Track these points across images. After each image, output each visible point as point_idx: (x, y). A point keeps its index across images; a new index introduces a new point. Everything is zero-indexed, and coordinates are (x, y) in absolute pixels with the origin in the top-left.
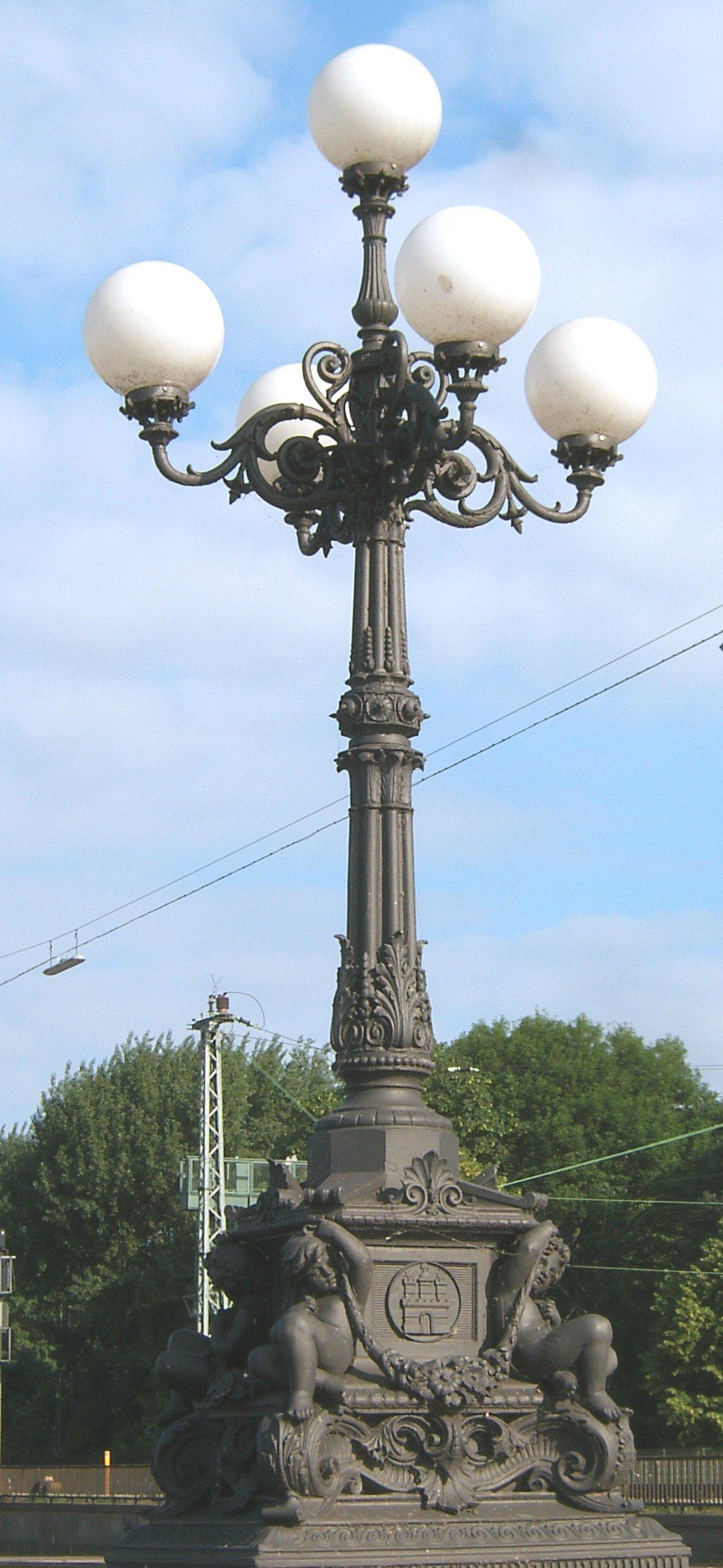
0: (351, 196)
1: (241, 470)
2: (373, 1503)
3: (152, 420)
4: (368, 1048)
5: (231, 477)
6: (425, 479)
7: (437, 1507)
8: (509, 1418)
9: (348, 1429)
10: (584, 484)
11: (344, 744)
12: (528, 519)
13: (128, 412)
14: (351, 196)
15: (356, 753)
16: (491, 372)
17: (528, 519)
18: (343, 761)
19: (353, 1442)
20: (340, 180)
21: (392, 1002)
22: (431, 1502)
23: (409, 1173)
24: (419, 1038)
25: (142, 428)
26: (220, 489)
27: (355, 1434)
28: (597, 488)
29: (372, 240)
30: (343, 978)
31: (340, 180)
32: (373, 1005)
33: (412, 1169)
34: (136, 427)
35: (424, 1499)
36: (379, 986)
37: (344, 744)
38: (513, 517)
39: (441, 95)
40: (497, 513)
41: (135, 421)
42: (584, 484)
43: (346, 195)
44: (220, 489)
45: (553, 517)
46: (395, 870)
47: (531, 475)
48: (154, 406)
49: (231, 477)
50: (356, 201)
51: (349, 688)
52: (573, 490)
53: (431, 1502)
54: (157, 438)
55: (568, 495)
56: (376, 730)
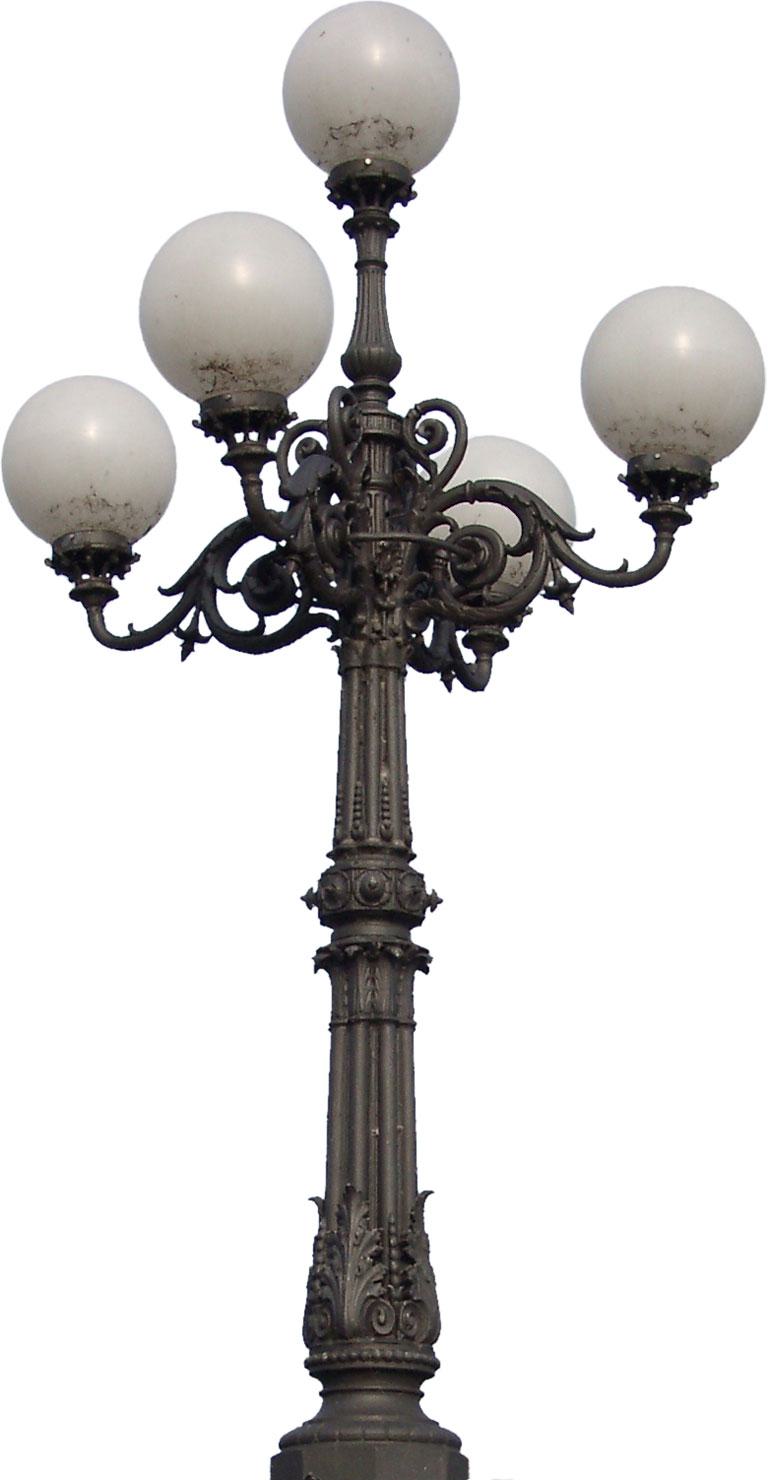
0: (639, 499)
1: (196, 616)
3: (85, 577)
5: (185, 625)
10: (665, 523)
11: (324, 936)
12: (588, 593)
13: (58, 564)
14: (639, 499)
15: (342, 947)
16: (328, 192)
17: (588, 593)
18: (325, 960)
25: (72, 586)
26: (172, 643)
28: (681, 529)
29: (370, 268)
30: (321, 1245)
34: (65, 585)
37: (324, 936)
38: (564, 595)
40: (541, 585)
41: (64, 579)
42: (665, 523)
43: (335, 206)
44: (172, 643)
45: (621, 579)
47: (621, 563)
49: (185, 625)
50: (348, 212)
51: (331, 863)
52: (649, 532)
54: (94, 599)
55: (639, 546)
56: (371, 918)
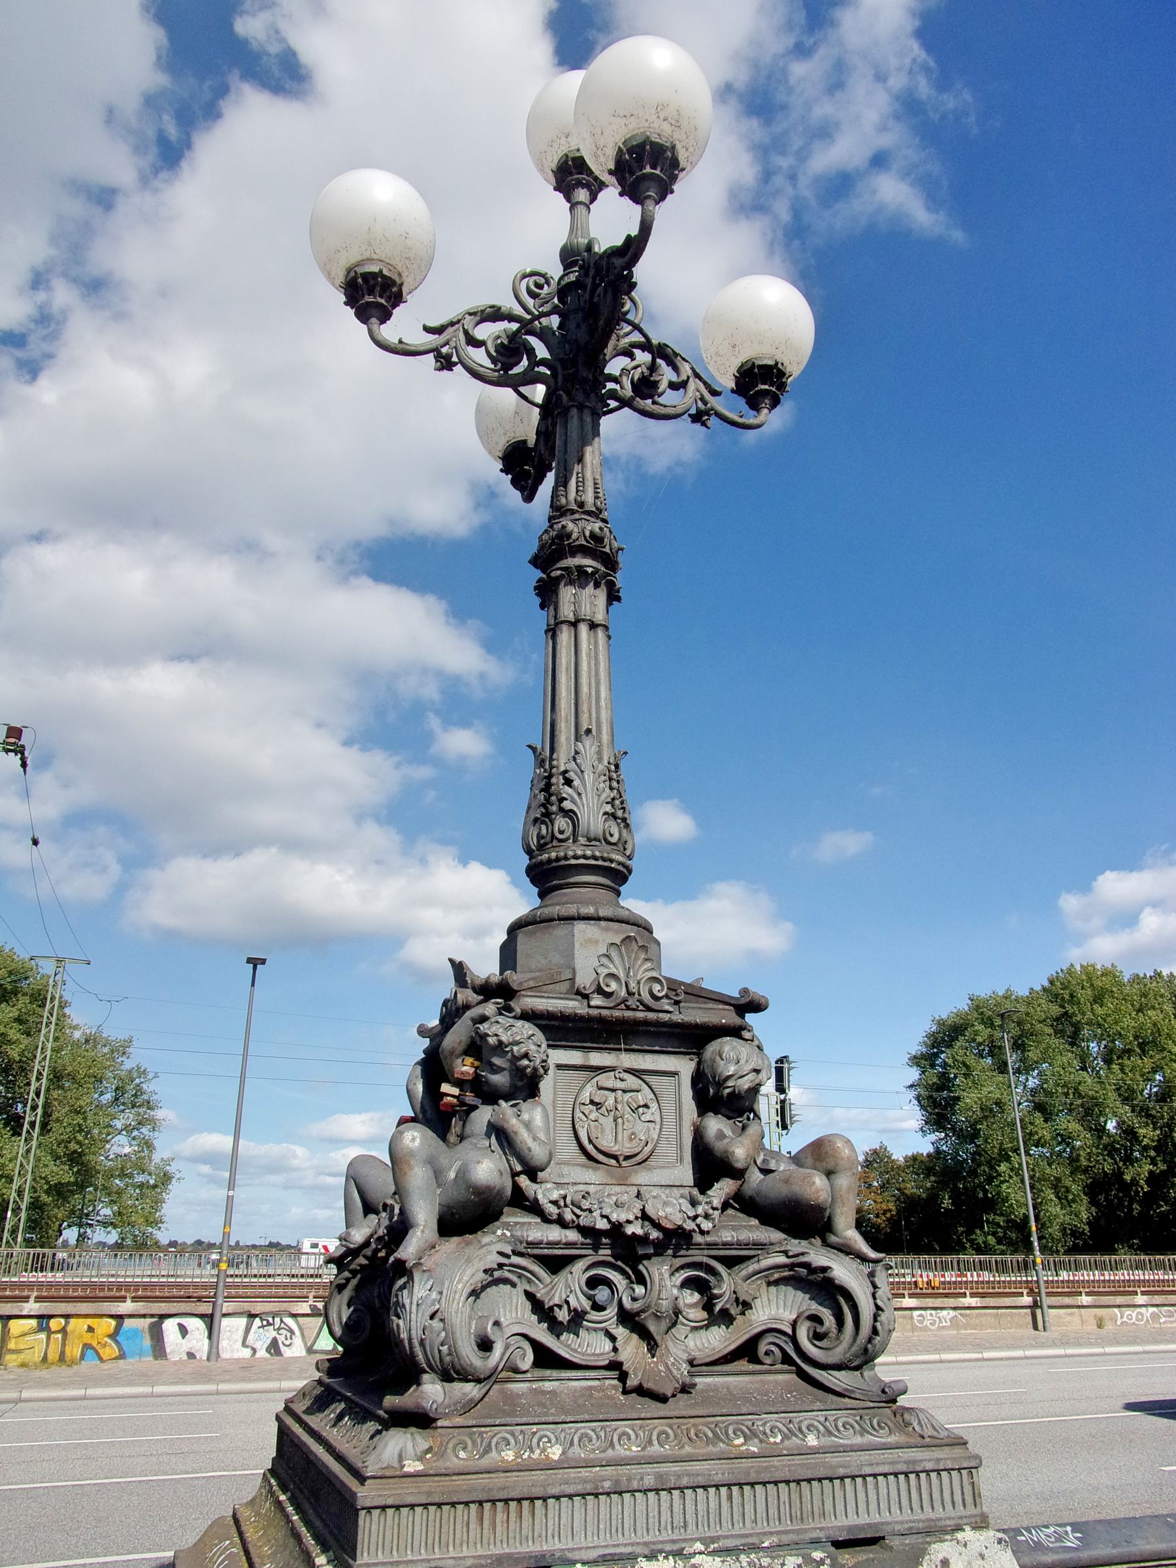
2: (555, 1383)
4: (555, 843)
6: (936, 62)
7: (641, 1391)
8: (731, 1262)
9: (520, 1276)
12: (713, 421)
19: (530, 1296)
20: (621, 195)
21: (579, 794)
22: (632, 1382)
23: (605, 960)
24: (611, 835)
27: (529, 1281)
31: (621, 195)
32: (562, 800)
33: (608, 956)
35: (623, 1377)
36: (569, 782)
39: (794, 284)
46: (563, 725)
48: (360, 280)
53: (632, 1382)
